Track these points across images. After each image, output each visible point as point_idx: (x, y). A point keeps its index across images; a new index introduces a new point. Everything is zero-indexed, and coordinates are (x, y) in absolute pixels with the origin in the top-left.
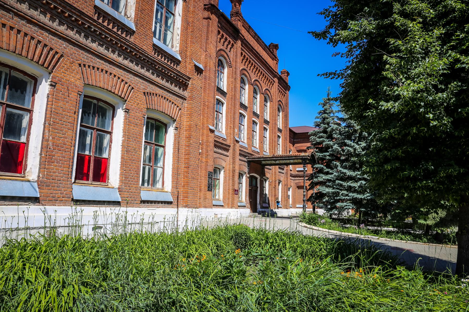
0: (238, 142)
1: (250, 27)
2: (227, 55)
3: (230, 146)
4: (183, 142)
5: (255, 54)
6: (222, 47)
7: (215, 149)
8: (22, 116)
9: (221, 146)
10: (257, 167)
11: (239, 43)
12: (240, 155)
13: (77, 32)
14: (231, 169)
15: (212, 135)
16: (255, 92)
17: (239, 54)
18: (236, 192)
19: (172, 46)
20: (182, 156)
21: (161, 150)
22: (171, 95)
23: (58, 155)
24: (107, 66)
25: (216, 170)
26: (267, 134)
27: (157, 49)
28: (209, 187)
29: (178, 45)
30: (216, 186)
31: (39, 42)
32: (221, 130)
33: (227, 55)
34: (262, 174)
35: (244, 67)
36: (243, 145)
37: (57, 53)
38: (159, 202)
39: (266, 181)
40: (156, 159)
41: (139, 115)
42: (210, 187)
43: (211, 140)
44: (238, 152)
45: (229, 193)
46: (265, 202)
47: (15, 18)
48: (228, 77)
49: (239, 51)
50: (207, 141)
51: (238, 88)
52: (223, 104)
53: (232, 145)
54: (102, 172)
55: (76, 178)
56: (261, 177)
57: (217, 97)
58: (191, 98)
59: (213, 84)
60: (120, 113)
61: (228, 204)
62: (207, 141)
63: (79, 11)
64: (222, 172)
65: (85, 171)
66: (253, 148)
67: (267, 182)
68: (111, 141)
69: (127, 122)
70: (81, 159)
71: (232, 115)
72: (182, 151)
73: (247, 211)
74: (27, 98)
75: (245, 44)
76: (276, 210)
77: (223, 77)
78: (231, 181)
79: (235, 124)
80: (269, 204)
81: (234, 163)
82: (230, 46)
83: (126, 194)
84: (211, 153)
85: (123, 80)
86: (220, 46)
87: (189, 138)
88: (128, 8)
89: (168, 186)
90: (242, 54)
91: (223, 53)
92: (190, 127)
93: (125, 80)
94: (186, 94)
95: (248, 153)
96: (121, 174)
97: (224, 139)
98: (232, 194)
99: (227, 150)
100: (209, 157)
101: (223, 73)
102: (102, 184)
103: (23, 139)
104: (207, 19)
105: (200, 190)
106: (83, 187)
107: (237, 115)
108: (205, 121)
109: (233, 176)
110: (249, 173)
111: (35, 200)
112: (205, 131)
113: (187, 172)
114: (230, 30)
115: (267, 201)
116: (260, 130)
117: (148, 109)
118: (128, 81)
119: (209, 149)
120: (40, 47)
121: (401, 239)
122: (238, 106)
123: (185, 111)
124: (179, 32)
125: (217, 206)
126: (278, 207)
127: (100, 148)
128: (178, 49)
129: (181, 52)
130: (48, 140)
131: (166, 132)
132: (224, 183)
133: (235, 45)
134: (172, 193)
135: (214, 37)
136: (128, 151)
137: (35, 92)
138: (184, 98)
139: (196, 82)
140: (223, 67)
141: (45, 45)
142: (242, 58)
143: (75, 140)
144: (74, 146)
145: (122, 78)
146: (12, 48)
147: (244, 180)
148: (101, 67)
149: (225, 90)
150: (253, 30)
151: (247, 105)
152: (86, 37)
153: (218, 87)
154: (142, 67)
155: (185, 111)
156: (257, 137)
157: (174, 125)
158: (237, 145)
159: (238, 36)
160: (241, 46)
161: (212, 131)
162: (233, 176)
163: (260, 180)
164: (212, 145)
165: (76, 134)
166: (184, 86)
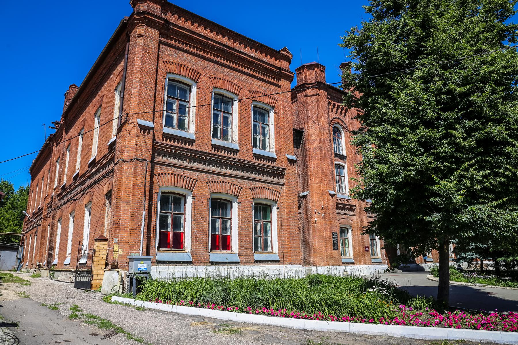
2: (342, 121)
3: (355, 206)
4: (285, 216)
6: (335, 116)
8: (180, 217)
13: (203, 164)
19: (270, 148)
21: (269, 224)
22: (271, 185)
23: (200, 237)
24: (223, 179)
25: (343, 230)
27: (257, 156)
28: (334, 247)
29: (274, 147)
31: (185, 177)
33: (342, 121)
37: (194, 180)
41: (248, 204)
42: (336, 246)
43: (332, 203)
45: (359, 250)
47: (173, 168)
48: (346, 141)
50: (329, 205)
52: (344, 167)
53: (357, 205)
54: (228, 244)
55: (211, 249)
57: (336, 162)
60: (235, 205)
61: (359, 261)
63: (203, 152)
65: (217, 244)
68: (231, 224)
69: (240, 210)
70: (214, 238)
74: (182, 207)
76: (423, 265)
82: (343, 112)
83: (243, 257)
84: (334, 215)
85: (234, 185)
86: (333, 115)
88: (234, 135)
89: (276, 250)
91: (336, 120)
92: (289, 204)
93: (236, 184)
94: (284, 181)
96: (239, 244)
98: (363, 251)
99: (353, 210)
101: (341, 139)
102: (228, 251)
103: (182, 230)
104: (316, 95)
106: (216, 254)
111: (190, 263)
117: (254, 199)
118: (238, 184)
119: (331, 212)
120: (185, 179)
125: (346, 263)
127: (225, 228)
128: (274, 149)
130: (194, 229)
131: (271, 211)
132: (353, 241)
136: (242, 229)
137: (185, 203)
138: (282, 185)
140: (340, 133)
141: (188, 177)
143: (209, 227)
144: (209, 231)
145: (233, 183)
146: (173, 184)
148: (219, 180)
152: (209, 165)
154: (247, 172)
155: (284, 194)
157: (276, 206)
161: (332, 196)
164: (334, 208)
165: (209, 223)
166: (282, 176)
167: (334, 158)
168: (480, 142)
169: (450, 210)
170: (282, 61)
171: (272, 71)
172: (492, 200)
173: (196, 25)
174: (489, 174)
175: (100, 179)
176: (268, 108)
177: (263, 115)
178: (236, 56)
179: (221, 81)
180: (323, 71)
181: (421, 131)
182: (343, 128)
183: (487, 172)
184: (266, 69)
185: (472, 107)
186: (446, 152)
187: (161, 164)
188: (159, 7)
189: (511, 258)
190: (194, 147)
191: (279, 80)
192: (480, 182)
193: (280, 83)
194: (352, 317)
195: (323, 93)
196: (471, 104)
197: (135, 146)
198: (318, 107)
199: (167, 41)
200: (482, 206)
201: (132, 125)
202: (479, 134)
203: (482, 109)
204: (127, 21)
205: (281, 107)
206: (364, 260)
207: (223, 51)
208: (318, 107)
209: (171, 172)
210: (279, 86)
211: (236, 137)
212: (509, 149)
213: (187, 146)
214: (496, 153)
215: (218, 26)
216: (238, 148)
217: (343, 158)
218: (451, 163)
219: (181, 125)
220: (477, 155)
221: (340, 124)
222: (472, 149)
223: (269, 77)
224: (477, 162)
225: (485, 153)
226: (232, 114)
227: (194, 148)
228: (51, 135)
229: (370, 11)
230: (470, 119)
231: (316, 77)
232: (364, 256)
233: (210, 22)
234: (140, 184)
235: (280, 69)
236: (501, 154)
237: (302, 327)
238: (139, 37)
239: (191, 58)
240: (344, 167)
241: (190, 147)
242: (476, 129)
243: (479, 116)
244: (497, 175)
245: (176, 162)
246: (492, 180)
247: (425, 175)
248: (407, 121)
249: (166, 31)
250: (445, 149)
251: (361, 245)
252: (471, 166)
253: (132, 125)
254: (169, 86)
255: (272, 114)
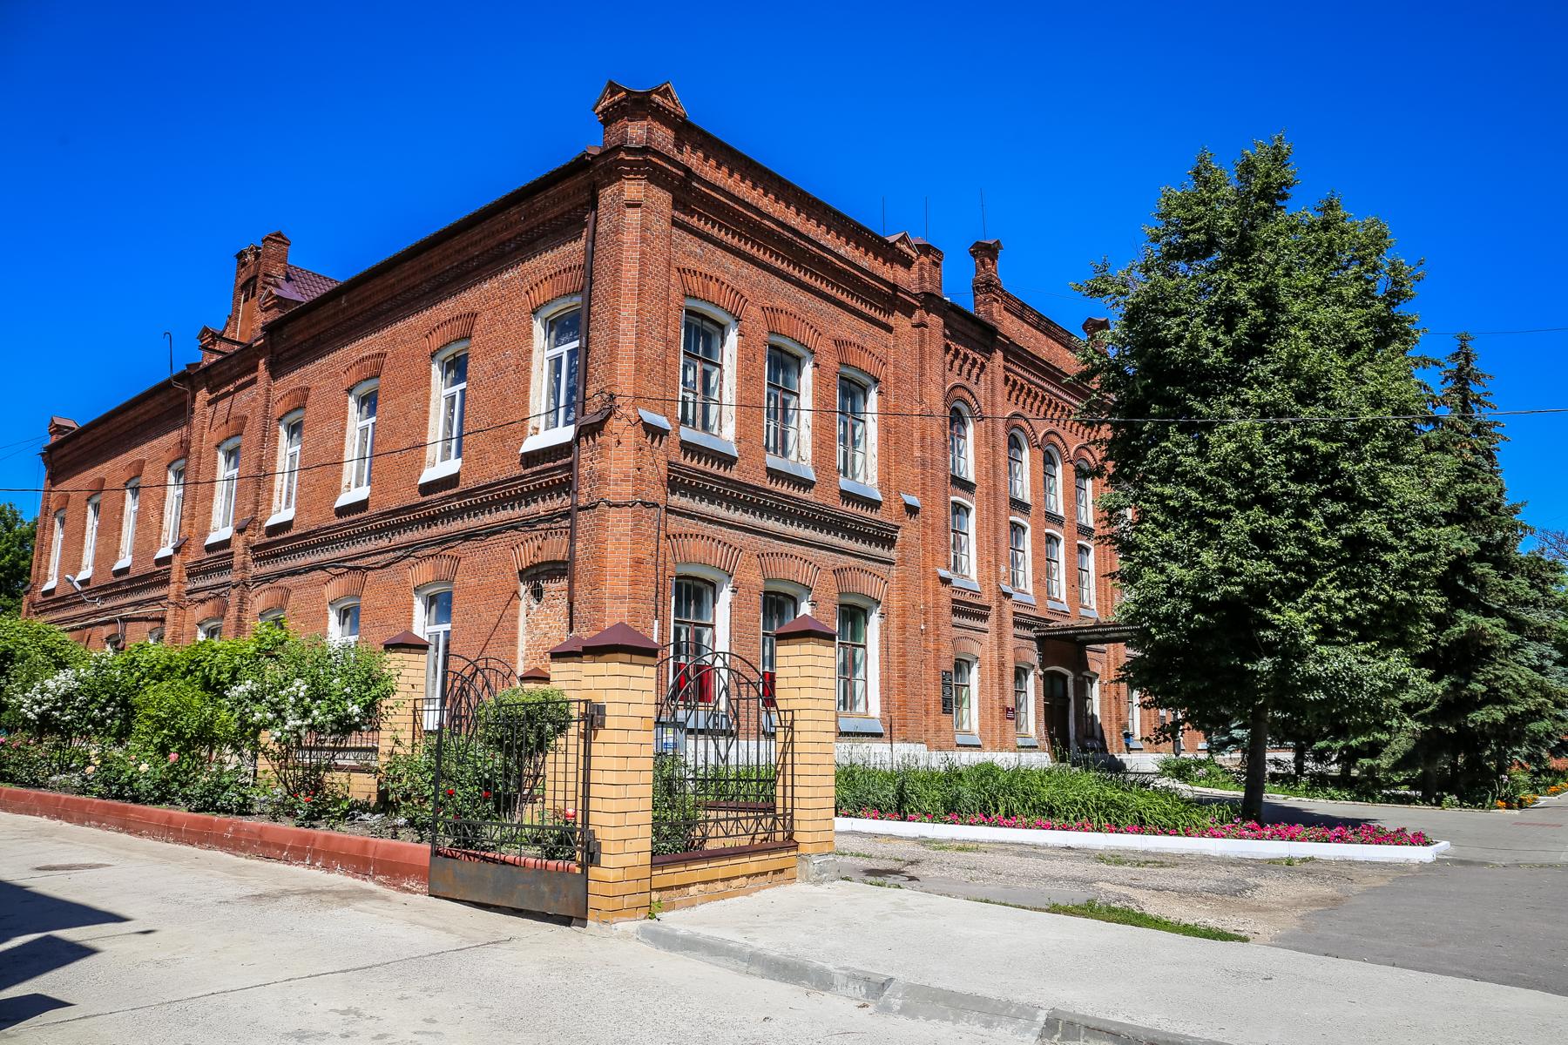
0: (1008, 595)
1: (1023, 305)
3: (989, 608)
4: (894, 636)
5: (1041, 370)
6: (957, 381)
7: (956, 620)
9: (969, 609)
10: (1064, 650)
11: (999, 354)
12: (1016, 624)
14: (996, 662)
15: (946, 589)
16: (1049, 460)
17: (999, 383)
18: (1012, 713)
19: (866, 477)
20: (894, 659)
21: (860, 651)
24: (710, 529)
25: (961, 666)
26: (1091, 561)
27: (774, 474)
30: (962, 701)
32: (966, 573)
34: (1080, 665)
35: (1015, 410)
36: (1025, 599)
38: (864, 734)
39: (1092, 681)
40: (855, 668)
41: (830, 606)
44: (1009, 619)
46: (1092, 737)
49: (1000, 374)
50: (936, 605)
51: (1002, 460)
52: (967, 510)
53: (994, 605)
56: (1077, 673)
57: (953, 498)
58: (903, 561)
59: (942, 475)
61: (992, 742)
62: (936, 605)
64: (975, 669)
66: (1051, 604)
67: (1096, 685)
71: (991, 533)
72: (894, 650)
73: (1041, 760)
75: (1015, 353)
76: (1124, 757)
77: (965, 445)
78: (996, 688)
79: (999, 552)
80: (1103, 740)
81: (1001, 646)
87: (903, 628)
89: (875, 709)
90: (1007, 379)
91: (959, 392)
92: (904, 608)
94: (893, 554)
95: (1038, 619)
97: (975, 594)
99: (984, 618)
100: (942, 639)
105: (927, 712)
107: (1005, 530)
108: (929, 560)
109: (1001, 676)
110: (1042, 667)
112: (930, 582)
113: (904, 685)
114: (973, 335)
115: (1098, 734)
116: (1068, 555)
119: (941, 622)
121: (1332, 798)
122: (1004, 505)
123: (894, 584)
124: (875, 450)
126: (1129, 750)
129: (884, 483)
131: (866, 622)
132: (981, 693)
133: (988, 365)
134: (882, 720)
135: (937, 362)
139: (909, 531)
140: (964, 424)
142: (1008, 388)
147: (1032, 683)
149: (971, 478)
150: (1032, 311)
151: (1028, 500)
153: (953, 477)
156: (1061, 576)
158: (1008, 603)
159: (994, 340)
160: (1003, 363)
161: (946, 581)
162: (1001, 676)
163: (1075, 681)
164: (947, 611)
167: (950, 488)
168: (1348, 541)
169: (1290, 651)
170: (897, 267)
171: (879, 291)
172: (1356, 640)
173: (713, 162)
174: (1356, 596)
175: (492, 531)
176: (866, 380)
177: (853, 396)
178: (813, 257)
179: (783, 317)
180: (937, 265)
181: (1257, 512)
182: (1061, 456)
183: (1353, 591)
184: (867, 286)
185: (1340, 477)
186: (1292, 555)
187: (679, 514)
188: (670, 134)
189: (1342, 743)
190: (733, 474)
191: (889, 312)
192: (1340, 609)
193: (891, 321)
194: (1141, 826)
195: (935, 320)
196: (1337, 473)
197: (633, 472)
198: (922, 358)
199: (686, 219)
200: (1340, 650)
201: (624, 422)
202: (1345, 530)
203: (1354, 483)
204: (594, 157)
205: (891, 379)
206: (1003, 741)
207: (789, 244)
208: (922, 358)
209: (695, 531)
210: (889, 329)
211: (807, 452)
212: (1387, 557)
213: (721, 472)
214: (1367, 560)
215: (780, 179)
216: (878, 496)
217: (967, 486)
218: (1299, 573)
219: (782, 447)
220: (1340, 563)
221: (966, 403)
222: (1332, 552)
223: (812, 274)
224: (1339, 573)
225: (1352, 561)
226: (798, 395)
227: (736, 477)
228: (189, 366)
229: (1156, 239)
230: (1335, 499)
231: (922, 278)
232: (1003, 731)
233: (766, 171)
234: (648, 558)
235: (894, 287)
236: (1373, 561)
237: (1063, 843)
238: (629, 206)
239: (729, 261)
240: (967, 510)
241: (727, 474)
242: (1342, 519)
243: (1348, 495)
244: (1365, 598)
245: (704, 507)
246: (1358, 608)
247: (1257, 593)
248: (1231, 493)
249: (687, 195)
250: (1289, 550)
251: (997, 704)
252: (1331, 581)
253: (624, 422)
254: (688, 326)
255: (873, 396)
